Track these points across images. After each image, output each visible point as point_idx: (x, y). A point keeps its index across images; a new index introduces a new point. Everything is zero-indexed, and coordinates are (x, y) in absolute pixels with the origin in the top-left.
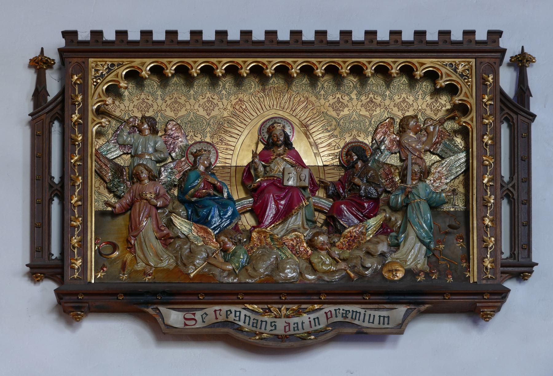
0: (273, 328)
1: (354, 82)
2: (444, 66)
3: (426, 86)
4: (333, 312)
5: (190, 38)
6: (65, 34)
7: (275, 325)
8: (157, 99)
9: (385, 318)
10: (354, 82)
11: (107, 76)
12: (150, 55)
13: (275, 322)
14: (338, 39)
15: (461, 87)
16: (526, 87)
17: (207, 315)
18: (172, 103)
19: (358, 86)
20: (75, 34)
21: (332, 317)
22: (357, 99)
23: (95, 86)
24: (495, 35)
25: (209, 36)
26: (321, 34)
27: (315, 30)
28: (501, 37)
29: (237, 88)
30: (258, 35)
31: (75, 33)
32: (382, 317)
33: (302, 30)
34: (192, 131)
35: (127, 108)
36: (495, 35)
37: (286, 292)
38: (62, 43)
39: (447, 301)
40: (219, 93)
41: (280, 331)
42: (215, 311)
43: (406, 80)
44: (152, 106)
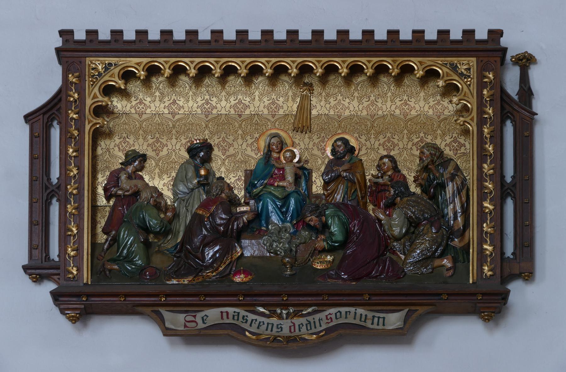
0: (280, 330)
1: (157, 84)
2: (444, 65)
3: (134, 87)
4: (344, 313)
5: (136, 37)
6: (62, 33)
7: (281, 327)
8: (386, 101)
9: (380, 319)
10: (157, 84)
11: (105, 75)
12: (185, 55)
13: (328, 323)
14: (386, 38)
15: (462, 88)
16: (527, 86)
17: (207, 316)
18: (270, 104)
19: (193, 87)
20: (121, 34)
21: (341, 317)
22: (260, 100)
23: (92, 85)
24: (495, 34)
25: (381, 35)
26: (368, 34)
27: (312, 30)
28: (502, 37)
29: (171, 89)
30: (305, 35)
31: (71, 32)
32: (376, 317)
33: (223, 30)
34: (455, 132)
35: (257, 109)
36: (495, 34)
37: (288, 293)
38: (59, 42)
39: (122, 302)
40: (152, 95)
41: (286, 331)
42: (222, 312)
43: (242, 81)
44: (248, 107)
